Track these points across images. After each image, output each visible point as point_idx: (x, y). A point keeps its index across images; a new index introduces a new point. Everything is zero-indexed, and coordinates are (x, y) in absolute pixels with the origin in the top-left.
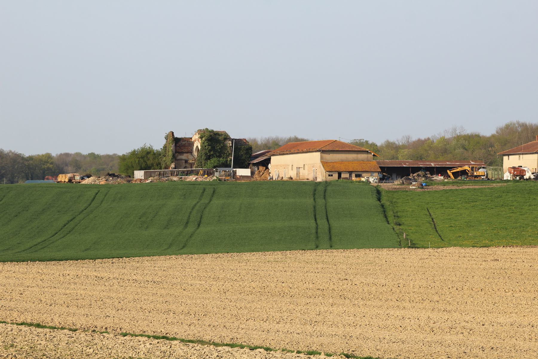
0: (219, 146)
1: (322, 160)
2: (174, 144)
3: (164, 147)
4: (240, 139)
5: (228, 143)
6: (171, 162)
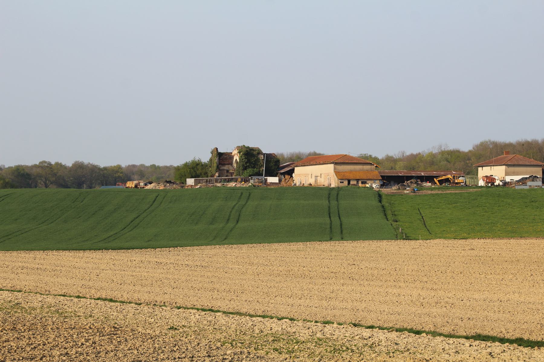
1: (335, 171)
2: (218, 158)
3: (210, 160)
4: (270, 154)
6: (215, 172)
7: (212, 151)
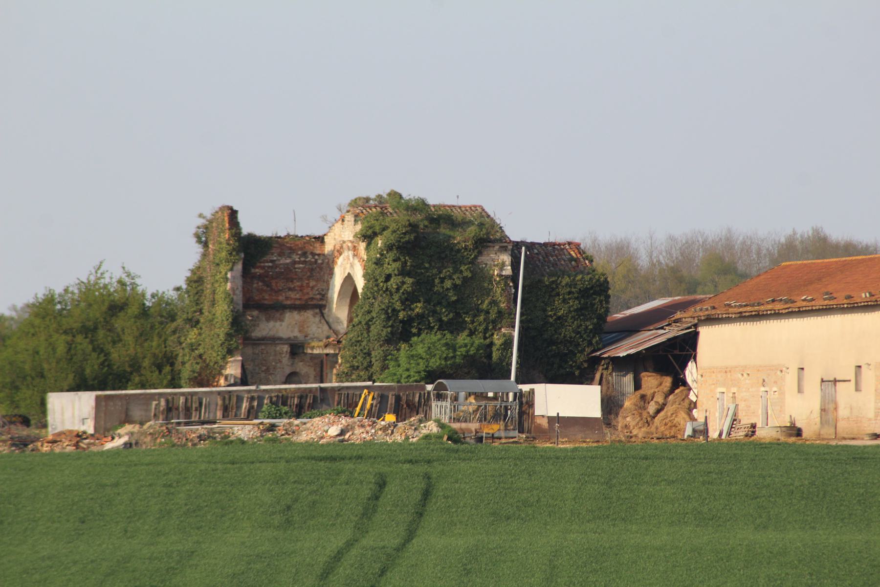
0: (450, 277)
2: (239, 267)
3: (189, 281)
4: (553, 245)
5: (493, 260)
7: (206, 227)
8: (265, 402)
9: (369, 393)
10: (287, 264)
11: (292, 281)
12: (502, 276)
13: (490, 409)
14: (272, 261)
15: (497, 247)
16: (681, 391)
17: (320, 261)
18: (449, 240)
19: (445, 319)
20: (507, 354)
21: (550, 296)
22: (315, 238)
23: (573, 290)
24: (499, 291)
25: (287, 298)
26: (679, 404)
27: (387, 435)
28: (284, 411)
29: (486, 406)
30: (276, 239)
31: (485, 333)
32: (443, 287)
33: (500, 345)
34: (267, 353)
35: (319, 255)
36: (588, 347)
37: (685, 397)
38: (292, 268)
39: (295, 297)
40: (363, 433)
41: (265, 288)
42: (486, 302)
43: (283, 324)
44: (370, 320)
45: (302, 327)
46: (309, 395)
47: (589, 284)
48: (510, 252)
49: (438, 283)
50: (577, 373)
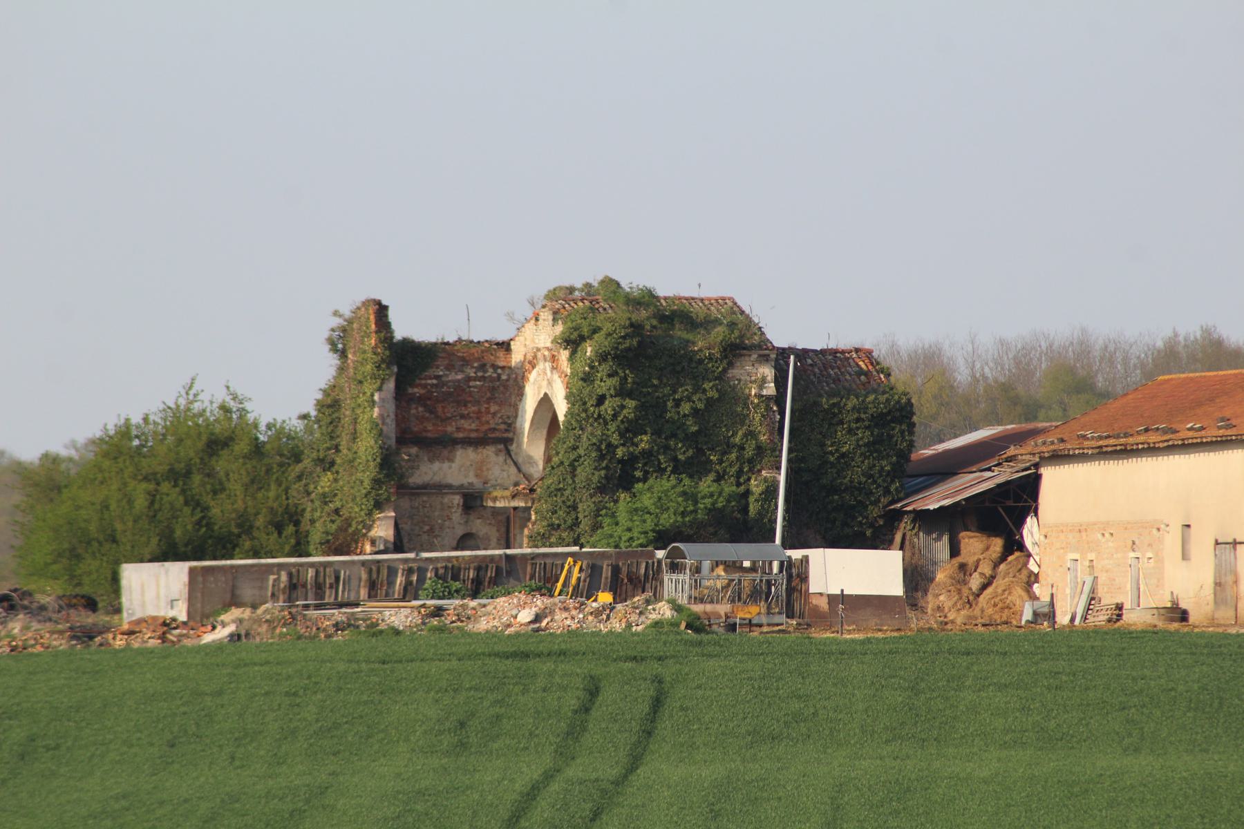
0: (689, 399)
2: (391, 385)
3: (320, 405)
4: (834, 352)
5: (749, 374)
7: (344, 330)
8: (429, 575)
9: (575, 562)
10: (459, 381)
11: (465, 406)
12: (763, 396)
13: (746, 584)
14: (437, 377)
15: (754, 356)
16: (1016, 559)
17: (504, 377)
18: (687, 346)
19: (681, 457)
20: (769, 507)
21: (831, 424)
22: (497, 344)
23: (863, 416)
24: (758, 417)
25: (458, 429)
26: (1014, 577)
27: (600, 622)
28: (454, 588)
29: (740, 581)
30: (443, 346)
31: (738, 477)
32: (678, 413)
33: (760, 495)
34: (431, 506)
35: (503, 368)
36: (884, 497)
37: (1022, 567)
38: (465, 387)
39: (469, 427)
40: (566, 618)
41: (427, 415)
42: (740, 433)
43: (453, 465)
44: (575, 460)
45: (480, 469)
46: (490, 565)
47: (886, 407)
48: (773, 363)
49: (592, 405)
50: (869, 533)
